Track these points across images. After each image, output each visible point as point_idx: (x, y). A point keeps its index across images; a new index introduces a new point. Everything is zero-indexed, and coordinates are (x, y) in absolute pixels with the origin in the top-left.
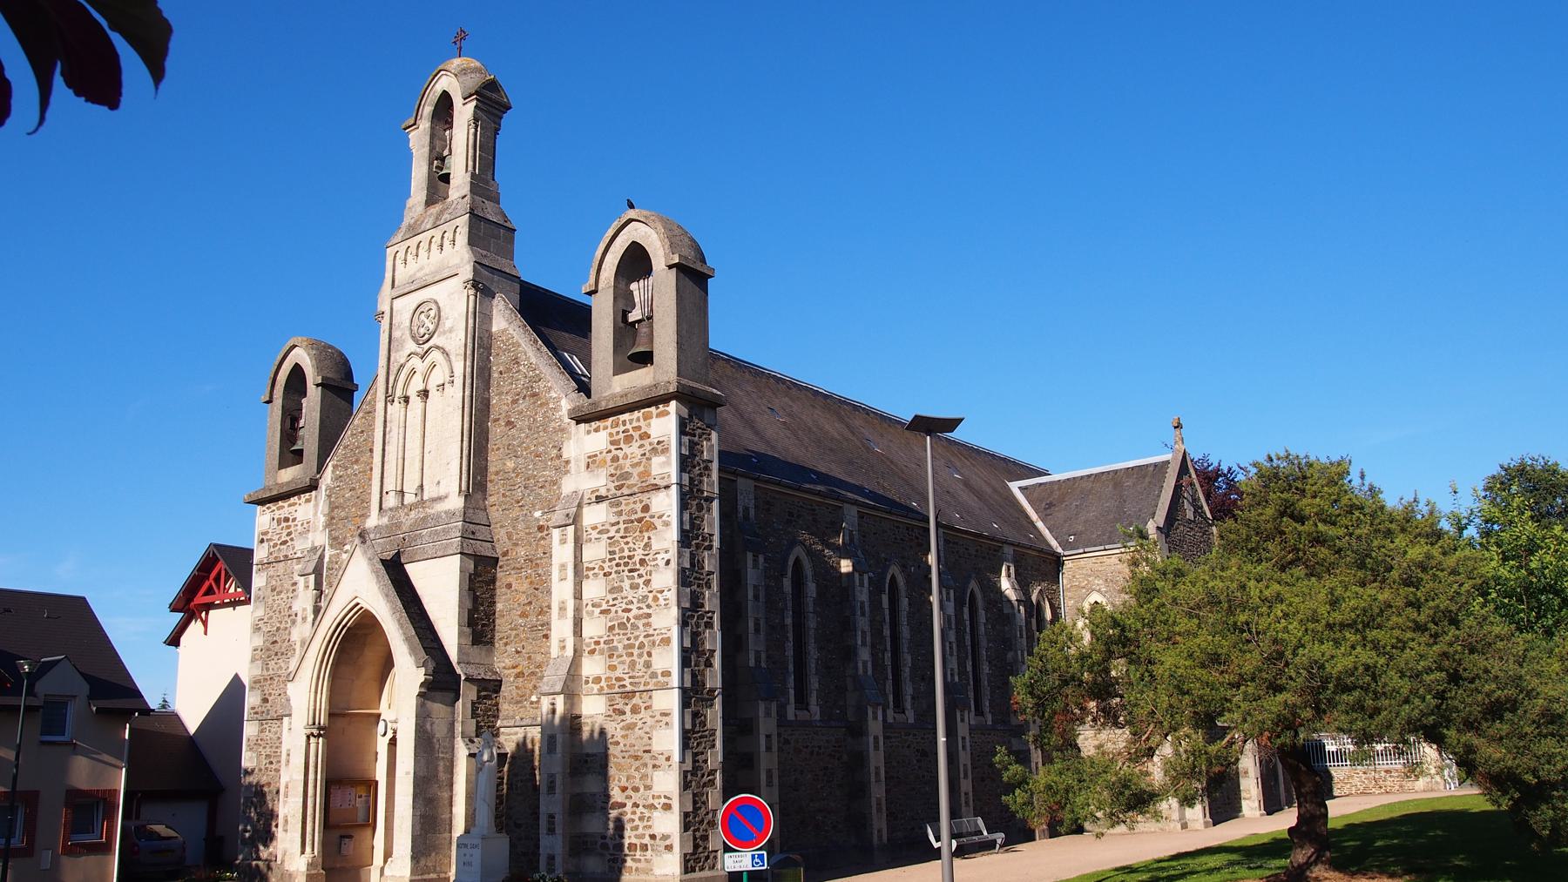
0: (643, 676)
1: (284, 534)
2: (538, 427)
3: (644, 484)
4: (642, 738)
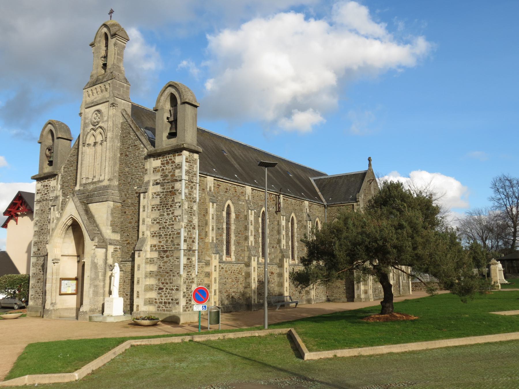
0: (170, 245)
1: (46, 191)
2: (136, 157)
3: (172, 179)
4: (169, 266)
